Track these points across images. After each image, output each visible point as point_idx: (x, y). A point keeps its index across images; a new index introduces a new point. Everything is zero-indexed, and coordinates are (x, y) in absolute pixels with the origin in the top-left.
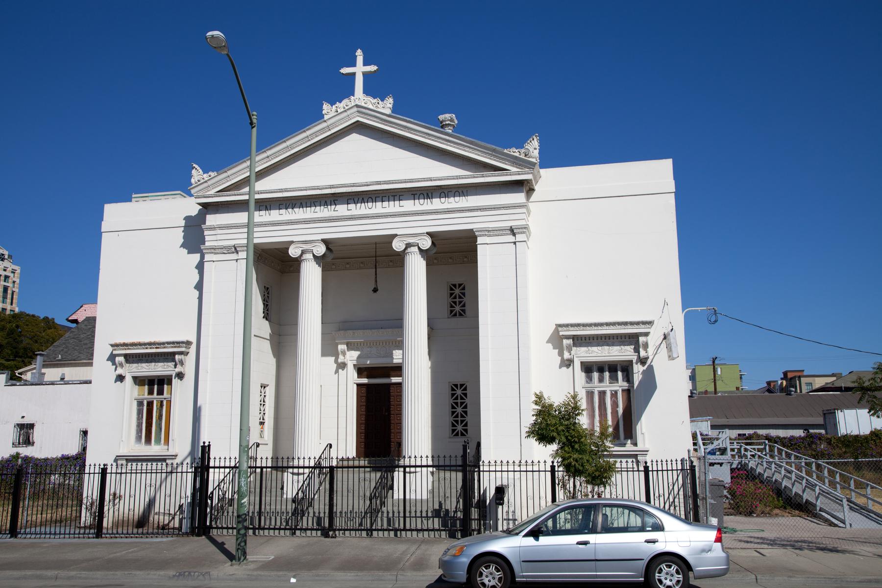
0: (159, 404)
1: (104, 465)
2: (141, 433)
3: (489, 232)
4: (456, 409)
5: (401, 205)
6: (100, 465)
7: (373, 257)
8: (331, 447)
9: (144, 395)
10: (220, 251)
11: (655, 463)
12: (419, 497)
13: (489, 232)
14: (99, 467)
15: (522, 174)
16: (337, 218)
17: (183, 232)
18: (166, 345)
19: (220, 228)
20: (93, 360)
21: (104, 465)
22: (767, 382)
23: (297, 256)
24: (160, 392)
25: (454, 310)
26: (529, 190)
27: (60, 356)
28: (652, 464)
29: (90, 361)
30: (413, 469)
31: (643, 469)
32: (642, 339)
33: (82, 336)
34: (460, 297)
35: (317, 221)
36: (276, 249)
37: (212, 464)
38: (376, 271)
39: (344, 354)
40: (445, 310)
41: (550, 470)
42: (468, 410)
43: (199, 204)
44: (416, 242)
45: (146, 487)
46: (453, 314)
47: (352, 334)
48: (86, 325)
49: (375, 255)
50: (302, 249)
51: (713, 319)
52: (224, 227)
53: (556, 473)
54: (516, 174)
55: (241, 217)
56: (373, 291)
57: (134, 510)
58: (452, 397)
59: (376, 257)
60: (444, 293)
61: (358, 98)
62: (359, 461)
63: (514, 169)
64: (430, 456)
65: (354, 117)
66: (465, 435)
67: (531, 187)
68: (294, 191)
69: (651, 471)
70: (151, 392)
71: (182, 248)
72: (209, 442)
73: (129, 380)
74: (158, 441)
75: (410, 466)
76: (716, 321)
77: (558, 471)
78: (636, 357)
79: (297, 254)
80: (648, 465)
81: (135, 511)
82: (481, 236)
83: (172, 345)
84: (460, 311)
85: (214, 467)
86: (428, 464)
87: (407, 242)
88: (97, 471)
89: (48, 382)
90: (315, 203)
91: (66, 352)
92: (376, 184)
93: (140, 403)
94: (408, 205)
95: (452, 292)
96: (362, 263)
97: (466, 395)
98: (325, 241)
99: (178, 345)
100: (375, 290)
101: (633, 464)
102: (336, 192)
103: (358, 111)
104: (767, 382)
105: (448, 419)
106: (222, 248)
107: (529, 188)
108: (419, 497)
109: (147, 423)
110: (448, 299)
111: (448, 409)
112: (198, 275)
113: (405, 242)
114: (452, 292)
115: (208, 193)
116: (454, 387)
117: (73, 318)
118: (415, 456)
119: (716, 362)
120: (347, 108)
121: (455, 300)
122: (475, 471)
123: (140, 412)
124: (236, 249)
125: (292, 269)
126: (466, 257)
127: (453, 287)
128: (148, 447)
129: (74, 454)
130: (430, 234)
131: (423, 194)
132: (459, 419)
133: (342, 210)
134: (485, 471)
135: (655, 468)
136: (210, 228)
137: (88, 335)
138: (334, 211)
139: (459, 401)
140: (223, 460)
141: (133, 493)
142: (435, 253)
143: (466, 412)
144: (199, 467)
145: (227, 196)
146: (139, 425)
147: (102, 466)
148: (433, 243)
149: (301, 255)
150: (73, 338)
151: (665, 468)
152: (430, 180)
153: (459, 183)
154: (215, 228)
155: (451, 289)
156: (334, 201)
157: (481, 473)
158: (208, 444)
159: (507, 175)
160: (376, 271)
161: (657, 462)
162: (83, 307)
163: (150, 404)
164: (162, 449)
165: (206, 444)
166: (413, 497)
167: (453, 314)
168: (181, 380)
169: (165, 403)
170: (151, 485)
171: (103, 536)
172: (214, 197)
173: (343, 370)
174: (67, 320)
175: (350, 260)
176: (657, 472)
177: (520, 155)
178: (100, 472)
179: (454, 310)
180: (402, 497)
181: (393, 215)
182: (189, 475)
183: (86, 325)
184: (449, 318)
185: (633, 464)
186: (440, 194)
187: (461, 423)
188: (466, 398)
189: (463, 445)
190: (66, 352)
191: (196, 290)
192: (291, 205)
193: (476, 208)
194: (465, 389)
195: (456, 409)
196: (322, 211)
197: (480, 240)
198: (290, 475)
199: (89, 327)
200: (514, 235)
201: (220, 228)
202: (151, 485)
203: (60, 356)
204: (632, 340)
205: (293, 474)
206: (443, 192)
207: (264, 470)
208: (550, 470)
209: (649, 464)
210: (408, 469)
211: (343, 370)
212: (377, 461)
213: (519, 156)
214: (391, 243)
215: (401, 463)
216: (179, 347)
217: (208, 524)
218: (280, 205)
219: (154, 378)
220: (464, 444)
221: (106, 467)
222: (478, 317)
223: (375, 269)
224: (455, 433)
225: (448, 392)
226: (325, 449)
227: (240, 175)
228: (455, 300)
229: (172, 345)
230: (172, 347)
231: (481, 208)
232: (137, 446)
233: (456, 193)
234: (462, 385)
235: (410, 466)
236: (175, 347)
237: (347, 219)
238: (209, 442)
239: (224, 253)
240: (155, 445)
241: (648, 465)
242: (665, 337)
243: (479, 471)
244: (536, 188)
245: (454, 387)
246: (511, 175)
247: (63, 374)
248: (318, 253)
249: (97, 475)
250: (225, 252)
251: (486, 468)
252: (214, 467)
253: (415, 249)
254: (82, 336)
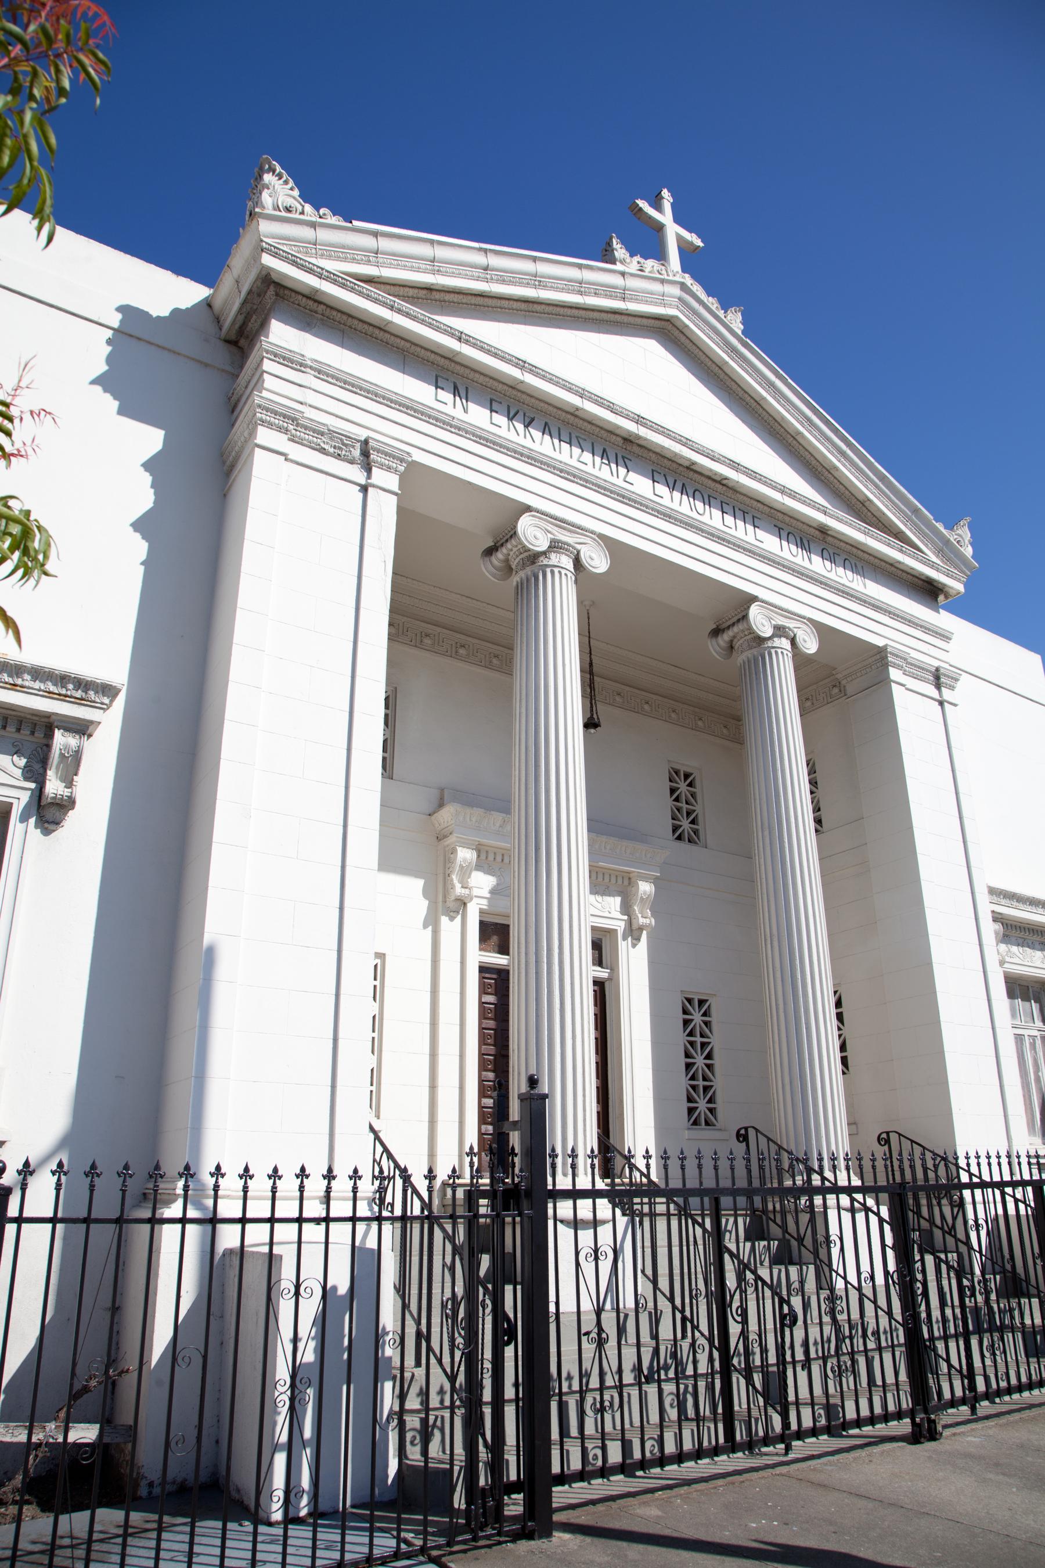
10: (309, 437)
16: (638, 499)
17: (109, 342)
18: (27, 680)
19: (319, 372)
32: (61, 740)
35: (593, 484)
39: (465, 873)
45: (578, 1264)
47: (498, 825)
52: (333, 377)
62: (53, 1220)
68: (550, 381)
71: (98, 389)
78: (25, 797)
79: (537, 543)
83: (52, 688)
99: (79, 694)
103: (680, 299)
106: (322, 434)
112: (152, 491)
113: (773, 622)
115: (313, 260)
124: (365, 454)
136: (284, 358)
154: (306, 366)
168: (47, 832)
173: (452, 919)
178: (10, 1229)
181: (750, 551)
191: (138, 536)
192: (521, 414)
193: (885, 606)
198: (565, 1234)
201: (319, 372)
205: (576, 1224)
211: (452, 919)
216: (80, 701)
227: (405, 268)
229: (52, 688)
230: (50, 695)
231: (892, 610)
236: (63, 698)
237: (658, 512)
250: (326, 447)
253: (567, 562)
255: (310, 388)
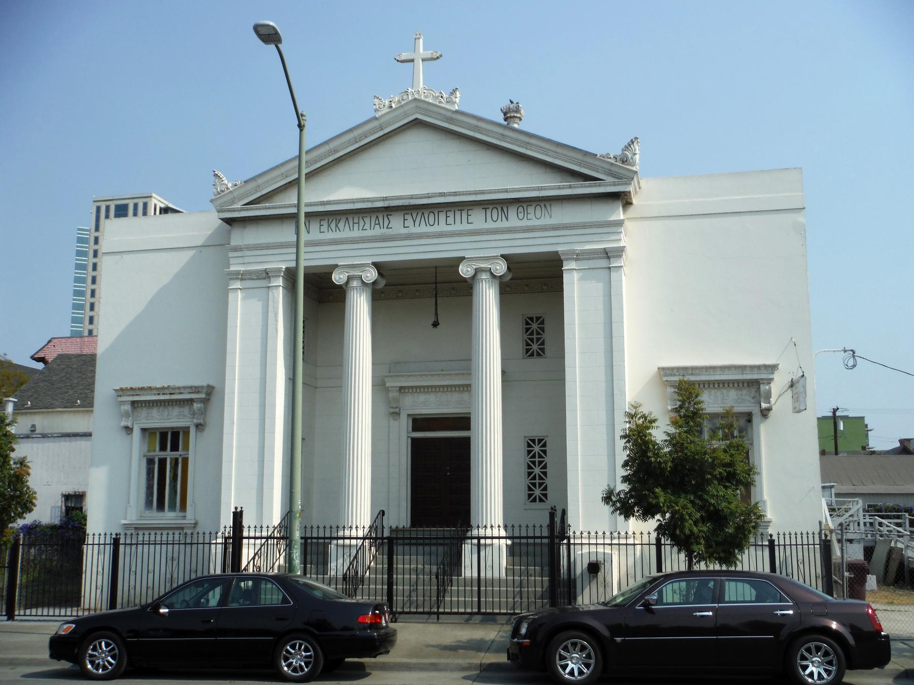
0: (173, 463)
1: (117, 535)
2: (152, 497)
3: (579, 256)
4: (539, 466)
5: (405, 226)
6: (111, 534)
7: (432, 284)
8: (383, 514)
9: (154, 451)
11: (781, 537)
12: (496, 575)
13: (579, 256)
14: (111, 537)
15: (618, 185)
20: (92, 407)
21: (117, 535)
22: (899, 440)
23: (342, 283)
24: (175, 448)
25: (531, 349)
26: (626, 204)
27: (79, 401)
28: (778, 537)
29: (91, 409)
30: (489, 541)
31: (767, 543)
32: (763, 388)
33: (55, 378)
34: (538, 333)
36: (313, 274)
37: (245, 534)
38: (436, 301)
40: (520, 347)
41: (655, 543)
42: (548, 470)
43: (223, 219)
44: (488, 266)
46: (529, 353)
48: (58, 365)
49: (435, 281)
50: (349, 274)
51: (851, 363)
53: (663, 547)
54: (611, 185)
55: (286, 233)
56: (432, 325)
57: (153, 588)
58: (528, 454)
59: (436, 283)
60: (520, 327)
61: (417, 90)
63: (610, 179)
64: (502, 525)
65: (412, 114)
66: (544, 501)
67: (629, 200)
69: (776, 545)
70: (163, 448)
72: (242, 508)
73: (137, 433)
74: (172, 507)
75: (485, 538)
76: (854, 366)
77: (665, 545)
79: (341, 280)
80: (773, 538)
81: (154, 589)
82: (567, 259)
84: (538, 350)
85: (249, 538)
86: (529, 535)
87: (477, 267)
88: (108, 542)
89: (55, 433)
90: (364, 218)
91: (36, 398)
92: (439, 196)
93: (150, 462)
94: (478, 220)
95: (528, 326)
96: (417, 291)
97: (545, 452)
98: (376, 265)
100: (436, 324)
101: (180, 537)
102: (391, 205)
104: (899, 440)
105: (522, 482)
107: (626, 202)
108: (496, 575)
109: (159, 484)
110: (523, 334)
111: (523, 470)
114: (528, 326)
116: (531, 443)
117: (39, 356)
118: (499, 525)
119: (838, 414)
120: (403, 103)
121: (532, 337)
122: (312, 542)
123: (150, 473)
125: (331, 298)
126: (546, 285)
127: (529, 321)
128: (161, 514)
129: (29, 524)
130: (504, 257)
131: (522, 207)
132: (537, 481)
133: (397, 225)
134: (621, 544)
135: (782, 543)
137: (62, 377)
138: (387, 228)
139: (537, 459)
140: (321, 530)
141: (151, 567)
142: (510, 280)
143: (545, 474)
144: (229, 538)
145: (257, 209)
146: (149, 488)
147: (114, 536)
148: (508, 268)
149: (347, 283)
150: (44, 381)
151: (96, 542)
152: (506, 191)
153: (446, 202)
155: (527, 323)
156: (387, 216)
157: (572, 547)
158: (240, 509)
159: (600, 186)
160: (436, 301)
161: (784, 534)
162: (52, 342)
163: (162, 462)
164: (178, 517)
165: (239, 510)
166: (489, 575)
167: (529, 353)
169: (180, 460)
170: (173, 558)
171: (16, 618)
172: (241, 211)
174: (33, 358)
175: (403, 287)
176: (785, 547)
177: (616, 161)
178: (112, 543)
179: (531, 349)
180: (475, 575)
182: (219, 546)
183: (58, 365)
184: (523, 358)
185: (180, 537)
186: (519, 207)
187: (540, 487)
188: (546, 455)
189: (550, 513)
190: (36, 398)
194: (544, 445)
195: (541, 469)
196: (372, 228)
197: (566, 266)
199: (63, 366)
200: (609, 258)
202: (173, 558)
203: (29, 403)
204: (755, 384)
206: (432, 212)
207: (309, 541)
208: (655, 543)
209: (775, 537)
210: (482, 541)
212: (425, 532)
213: (616, 163)
214: (458, 266)
215: (475, 533)
217: (711, 613)
218: (440, 213)
219: (166, 431)
220: (550, 511)
221: (118, 536)
222: (564, 357)
223: (434, 298)
224: (532, 499)
225: (523, 449)
226: (377, 517)
228: (532, 337)
232: (147, 512)
233: (537, 207)
234: (540, 441)
235: (485, 538)
238: (242, 508)
239: (253, 279)
240: (169, 511)
241: (773, 538)
242: (792, 385)
243: (569, 544)
244: (634, 201)
245: (531, 443)
246: (605, 186)
247: (34, 426)
248: (368, 279)
249: (108, 547)
250: (254, 277)
251: (578, 541)
252: (249, 538)
254: (55, 378)
255: (246, 256)
